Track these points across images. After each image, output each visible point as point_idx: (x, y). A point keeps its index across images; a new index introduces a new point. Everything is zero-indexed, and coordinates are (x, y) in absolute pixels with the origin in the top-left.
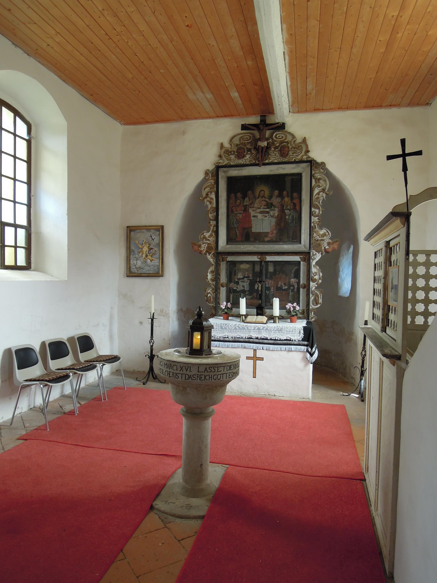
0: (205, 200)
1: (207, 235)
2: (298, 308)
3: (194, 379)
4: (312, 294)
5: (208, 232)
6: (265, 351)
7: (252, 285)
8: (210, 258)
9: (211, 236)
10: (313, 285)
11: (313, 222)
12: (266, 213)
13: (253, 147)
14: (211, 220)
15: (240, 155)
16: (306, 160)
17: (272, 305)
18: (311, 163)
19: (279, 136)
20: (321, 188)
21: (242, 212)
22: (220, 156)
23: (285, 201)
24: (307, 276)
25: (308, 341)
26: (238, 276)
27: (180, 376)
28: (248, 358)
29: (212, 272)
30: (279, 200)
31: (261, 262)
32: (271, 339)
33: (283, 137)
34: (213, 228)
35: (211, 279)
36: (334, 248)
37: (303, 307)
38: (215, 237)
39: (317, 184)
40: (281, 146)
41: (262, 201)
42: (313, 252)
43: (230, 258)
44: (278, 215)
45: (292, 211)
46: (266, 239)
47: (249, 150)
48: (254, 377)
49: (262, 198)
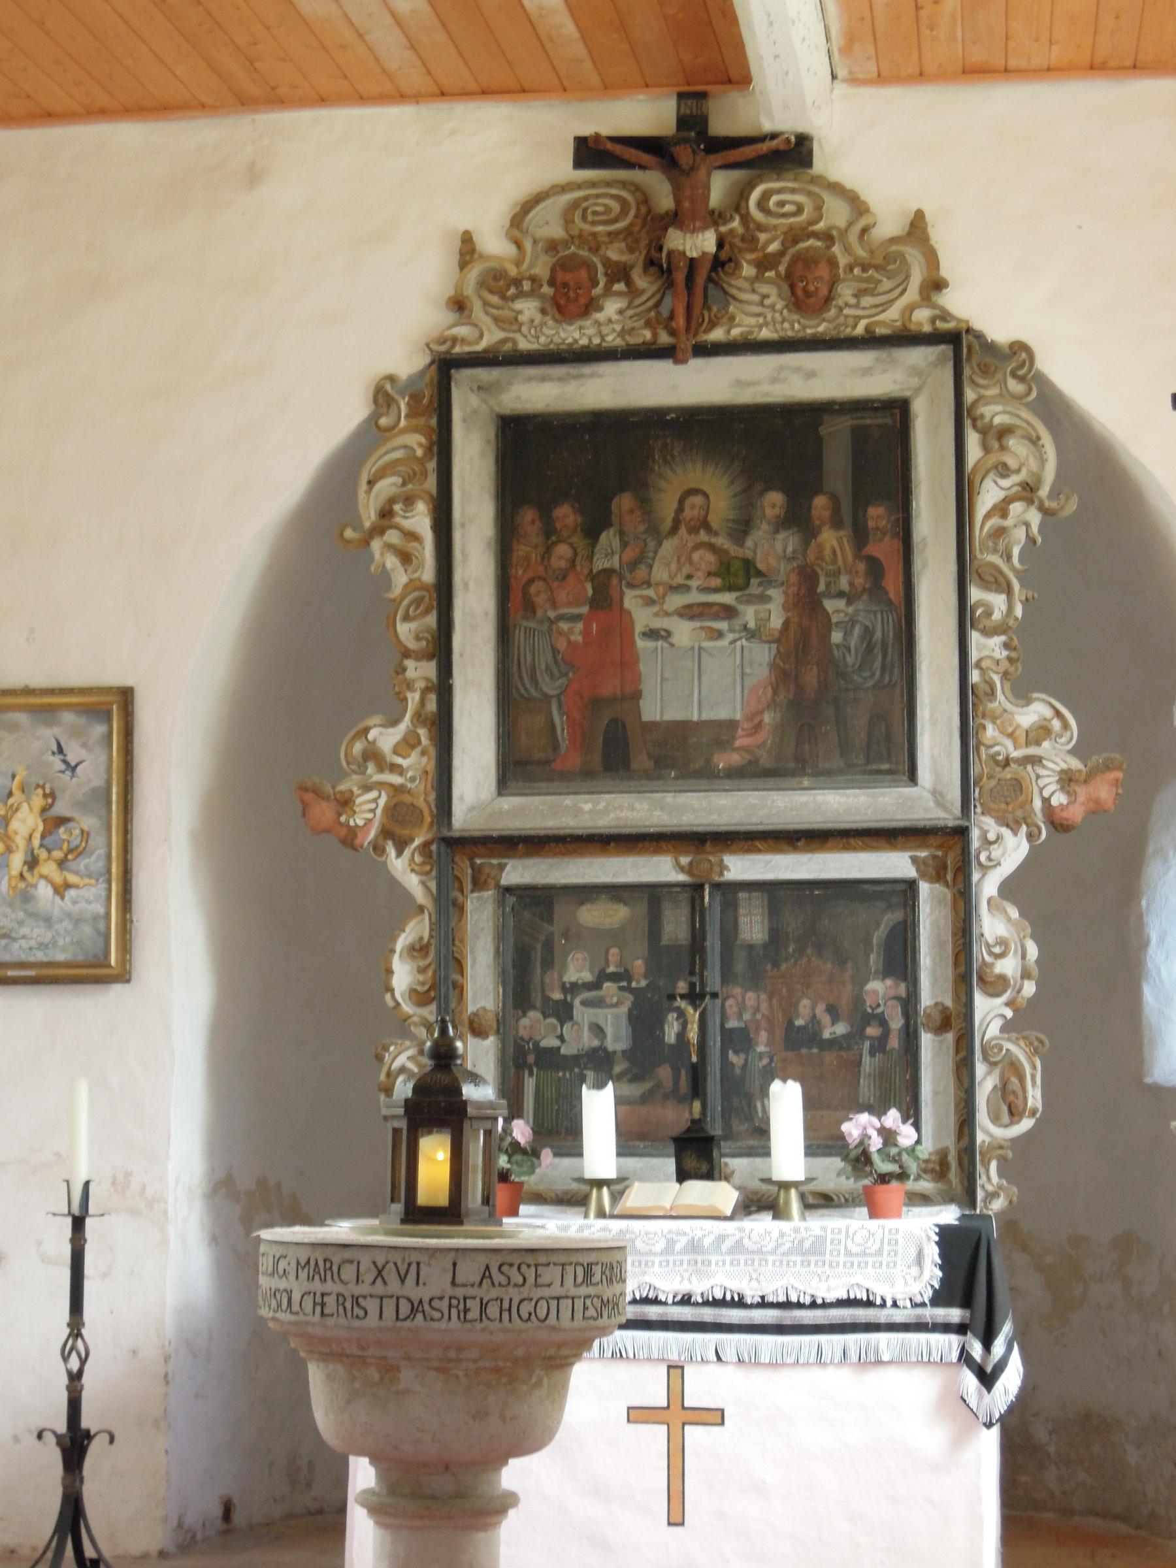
0: (376, 545)
1: (386, 738)
2: (907, 1135)
3: (437, 1315)
4: (986, 1058)
5: (394, 722)
6: (729, 1373)
7: (646, 1020)
8: (404, 869)
9: (409, 743)
10: (989, 1012)
11: (978, 665)
12: (716, 617)
13: (638, 259)
14: (407, 654)
15: (569, 300)
16: (927, 328)
17: (763, 1132)
18: (957, 343)
19: (781, 204)
20: (1015, 479)
21: (584, 610)
22: (459, 305)
23: (820, 547)
24: (956, 964)
25: (966, 1302)
26: (564, 968)
27: (372, 1306)
28: (638, 1414)
29: (417, 950)
30: (788, 541)
31: (698, 888)
32: (763, 1304)
33: (800, 210)
34: (422, 701)
35: (413, 992)
36: (1097, 802)
37: (937, 1135)
38: (432, 751)
39: (993, 459)
40: (791, 251)
41: (696, 547)
42: (984, 825)
43: (519, 872)
44: (786, 624)
45: (860, 605)
46: (722, 761)
47: (619, 273)
48: (676, 1520)
49: (693, 530)
